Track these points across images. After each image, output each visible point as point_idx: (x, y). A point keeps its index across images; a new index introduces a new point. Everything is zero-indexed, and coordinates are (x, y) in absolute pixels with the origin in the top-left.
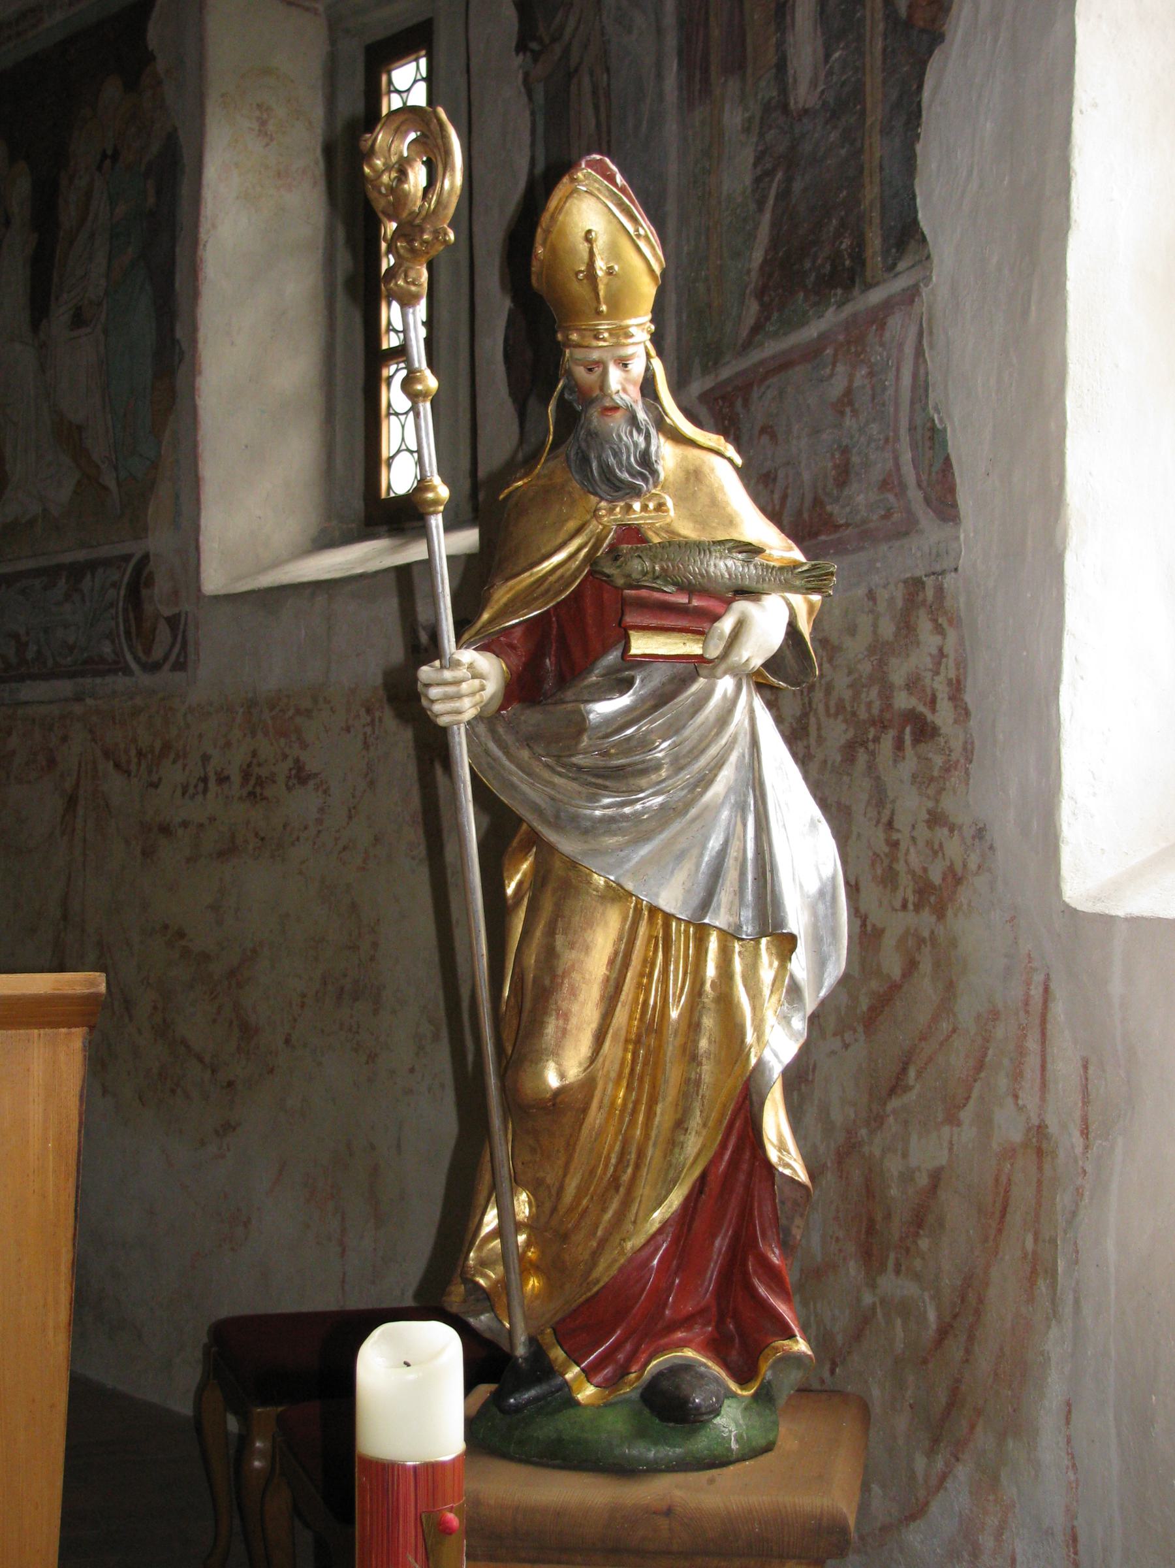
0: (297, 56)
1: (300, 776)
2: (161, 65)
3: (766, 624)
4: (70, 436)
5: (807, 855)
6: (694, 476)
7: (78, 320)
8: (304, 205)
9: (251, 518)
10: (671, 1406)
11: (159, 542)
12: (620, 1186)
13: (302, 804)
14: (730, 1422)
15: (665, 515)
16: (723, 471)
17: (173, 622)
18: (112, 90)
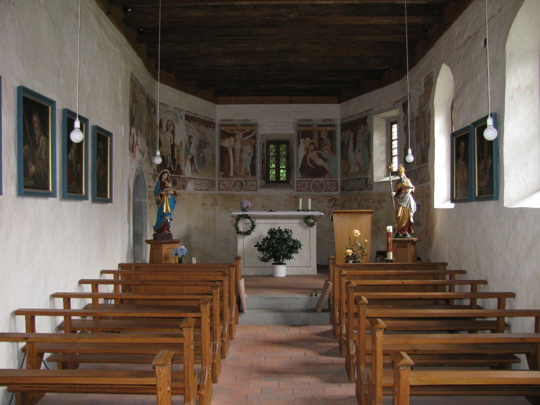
0: (383, 123)
1: (384, 201)
2: (368, 124)
3: (410, 191)
4: (358, 164)
5: (413, 204)
6: (407, 182)
7: (359, 151)
8: (384, 140)
9: (379, 174)
10: (405, 235)
11: (369, 176)
12: (402, 223)
13: (385, 204)
14: (408, 236)
15: (405, 184)
16: (409, 181)
17: (371, 185)
18: (363, 126)
